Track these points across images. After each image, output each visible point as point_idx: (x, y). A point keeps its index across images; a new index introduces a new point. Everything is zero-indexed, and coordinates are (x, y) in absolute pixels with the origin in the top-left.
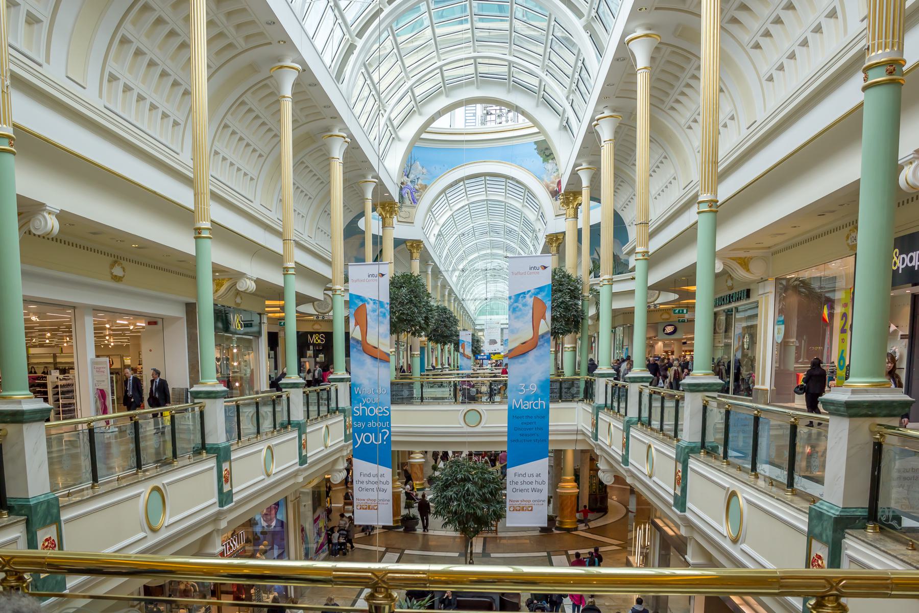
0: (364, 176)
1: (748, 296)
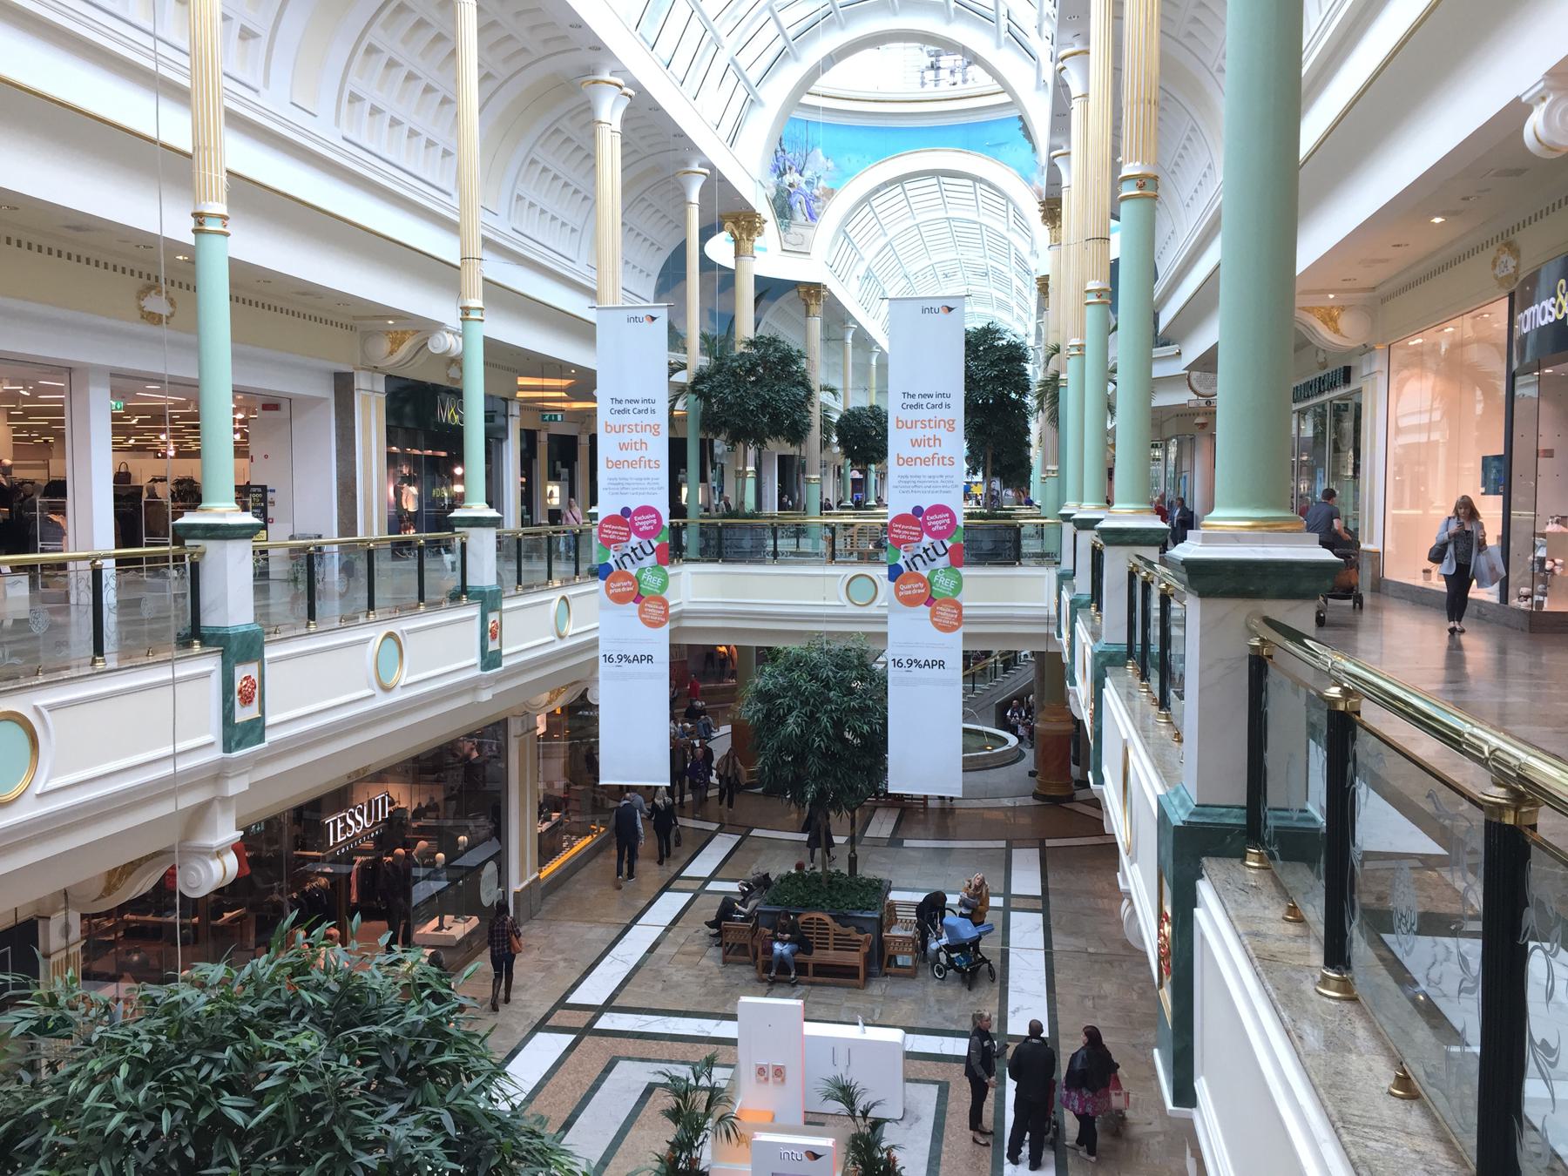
0: (686, 163)
1: (1347, 380)
